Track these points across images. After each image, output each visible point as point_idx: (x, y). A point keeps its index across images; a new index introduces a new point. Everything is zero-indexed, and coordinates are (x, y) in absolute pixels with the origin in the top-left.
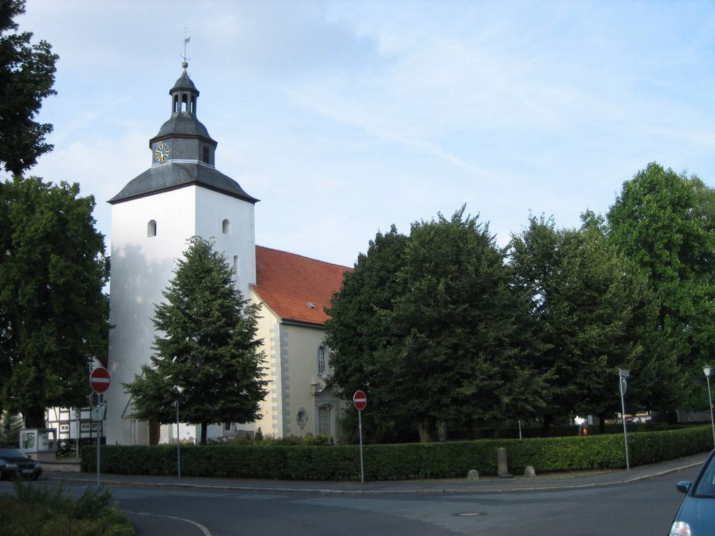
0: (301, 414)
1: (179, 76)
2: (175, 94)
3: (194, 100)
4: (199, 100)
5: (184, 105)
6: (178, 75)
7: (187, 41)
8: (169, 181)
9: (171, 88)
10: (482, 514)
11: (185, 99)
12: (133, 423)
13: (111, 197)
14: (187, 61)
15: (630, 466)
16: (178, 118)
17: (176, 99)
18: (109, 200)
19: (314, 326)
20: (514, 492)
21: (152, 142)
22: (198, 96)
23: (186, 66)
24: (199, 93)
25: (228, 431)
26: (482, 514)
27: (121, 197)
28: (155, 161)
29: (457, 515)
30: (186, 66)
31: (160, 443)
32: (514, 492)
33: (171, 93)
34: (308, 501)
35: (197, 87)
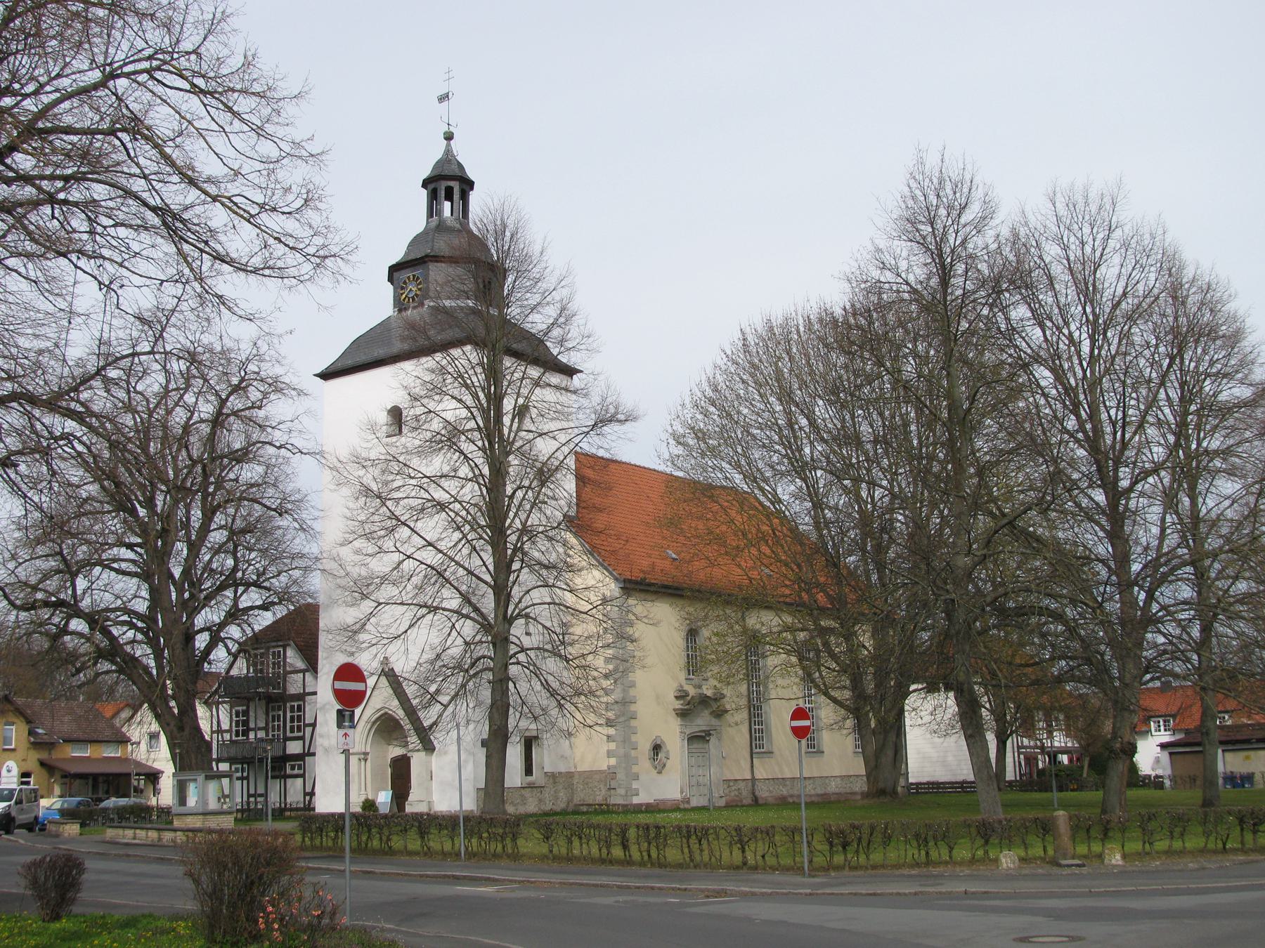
0: (657, 748)
1: (438, 154)
2: (431, 186)
3: (464, 197)
4: (474, 197)
5: (447, 205)
6: (437, 153)
7: (444, 98)
8: (398, 347)
9: (425, 177)
10: (1073, 939)
11: (449, 197)
12: (363, 763)
13: (323, 365)
14: (452, 129)
15: (353, 851)
16: (437, 228)
17: (433, 197)
18: (318, 371)
19: (670, 591)
20: (1099, 894)
21: (394, 270)
22: (472, 188)
23: (449, 137)
24: (473, 183)
25: (529, 779)
26: (1073, 939)
27: (350, 362)
28: (400, 305)
29: (1023, 940)
30: (449, 137)
31: (971, 778)
32: (1099, 894)
33: (425, 184)
34: (688, 910)
35: (471, 174)
